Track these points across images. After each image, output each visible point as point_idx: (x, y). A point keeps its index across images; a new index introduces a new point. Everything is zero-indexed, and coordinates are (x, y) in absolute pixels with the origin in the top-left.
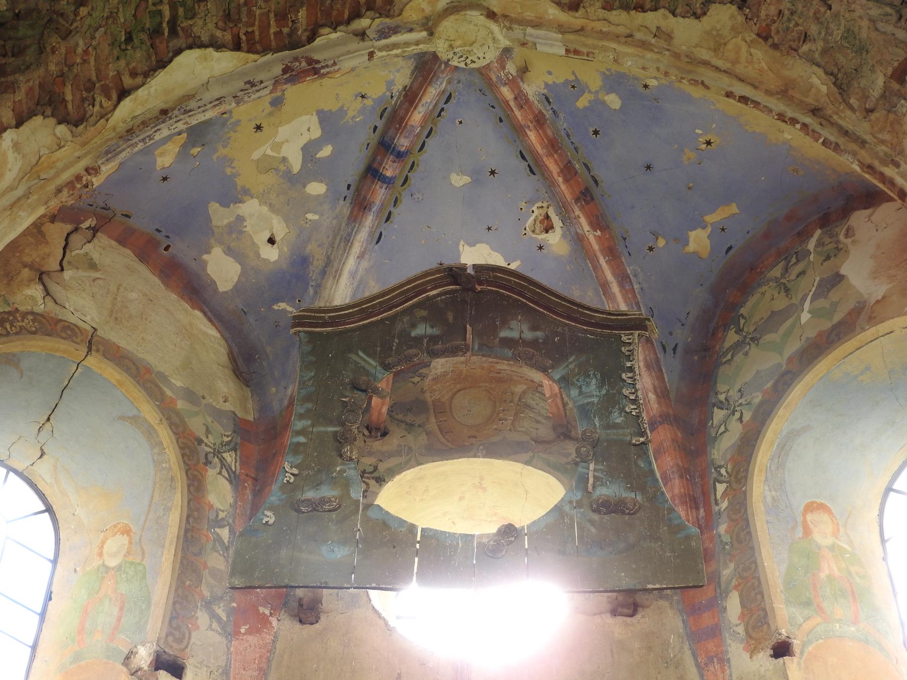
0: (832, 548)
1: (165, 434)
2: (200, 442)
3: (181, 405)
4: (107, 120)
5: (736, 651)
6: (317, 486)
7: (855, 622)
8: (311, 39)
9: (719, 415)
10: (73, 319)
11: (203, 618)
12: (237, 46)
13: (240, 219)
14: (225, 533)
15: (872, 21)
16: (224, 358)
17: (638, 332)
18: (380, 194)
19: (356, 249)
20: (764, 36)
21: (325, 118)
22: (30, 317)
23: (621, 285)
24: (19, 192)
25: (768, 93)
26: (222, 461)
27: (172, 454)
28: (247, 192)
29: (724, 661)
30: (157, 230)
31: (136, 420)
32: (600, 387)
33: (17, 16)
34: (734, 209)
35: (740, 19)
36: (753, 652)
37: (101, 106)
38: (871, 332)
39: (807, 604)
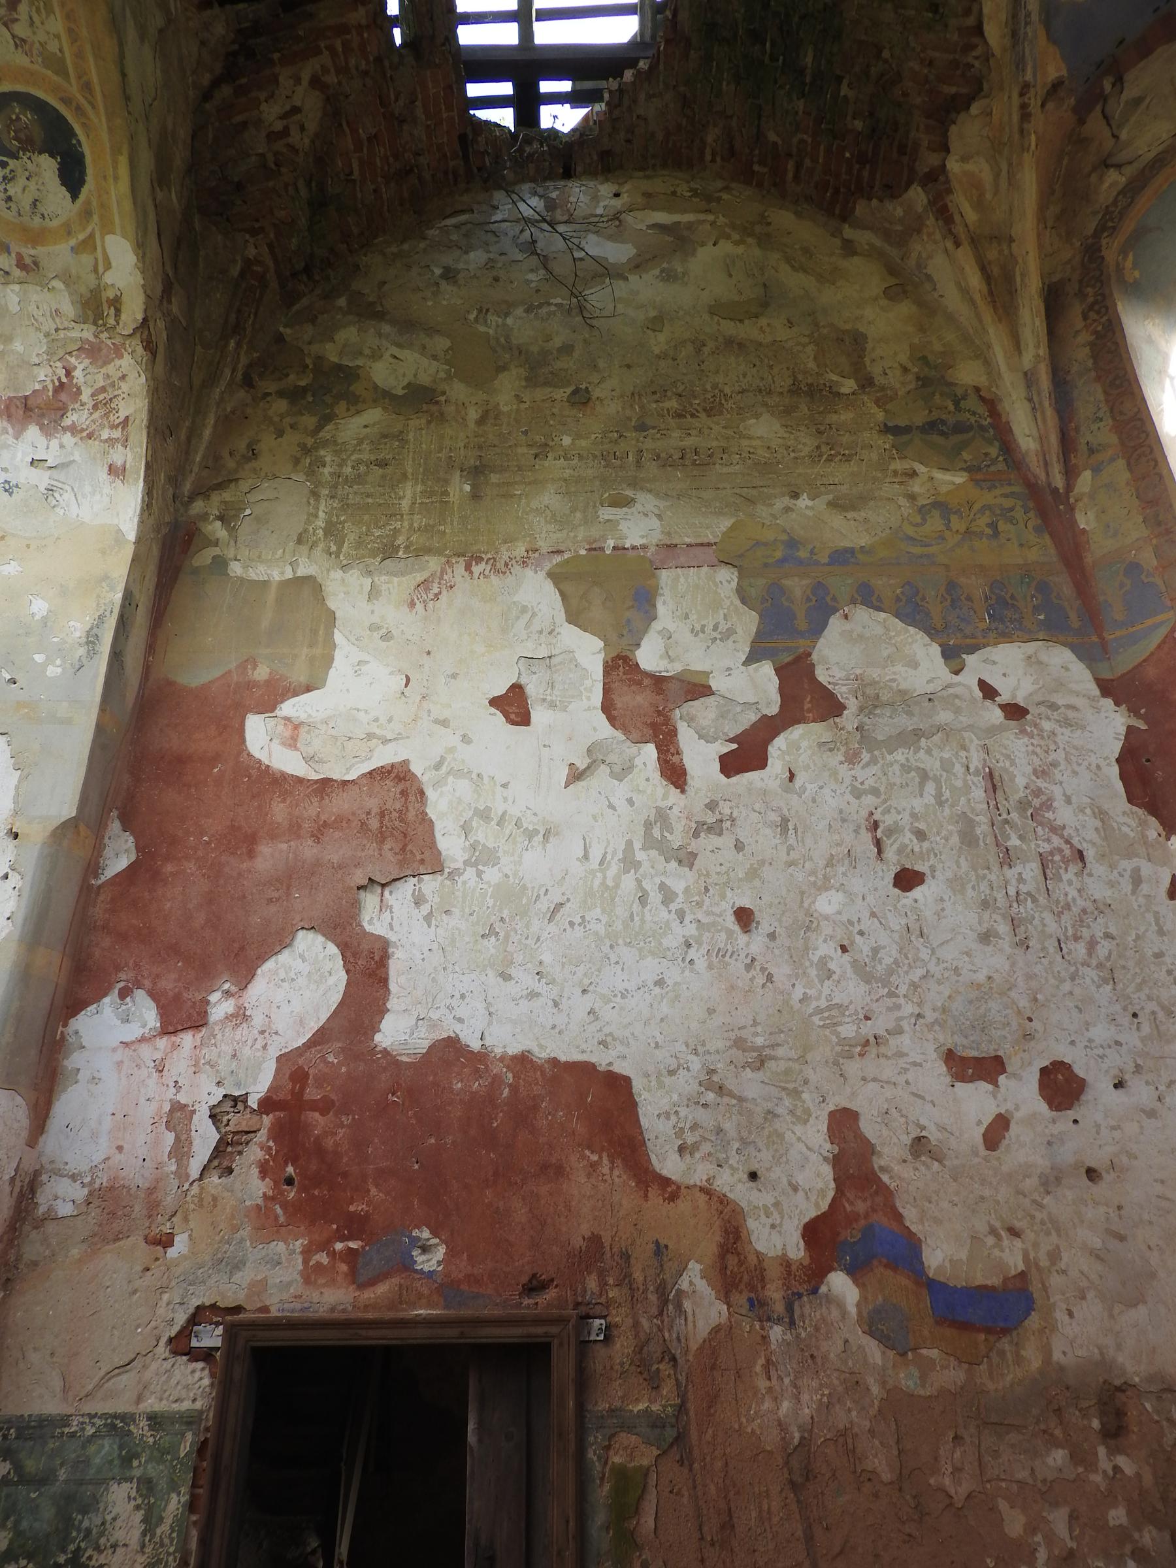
4: (993, 55)
17: (810, 140)
22: (1120, 197)
24: (1004, 166)
30: (1155, 11)
37: (976, 58)
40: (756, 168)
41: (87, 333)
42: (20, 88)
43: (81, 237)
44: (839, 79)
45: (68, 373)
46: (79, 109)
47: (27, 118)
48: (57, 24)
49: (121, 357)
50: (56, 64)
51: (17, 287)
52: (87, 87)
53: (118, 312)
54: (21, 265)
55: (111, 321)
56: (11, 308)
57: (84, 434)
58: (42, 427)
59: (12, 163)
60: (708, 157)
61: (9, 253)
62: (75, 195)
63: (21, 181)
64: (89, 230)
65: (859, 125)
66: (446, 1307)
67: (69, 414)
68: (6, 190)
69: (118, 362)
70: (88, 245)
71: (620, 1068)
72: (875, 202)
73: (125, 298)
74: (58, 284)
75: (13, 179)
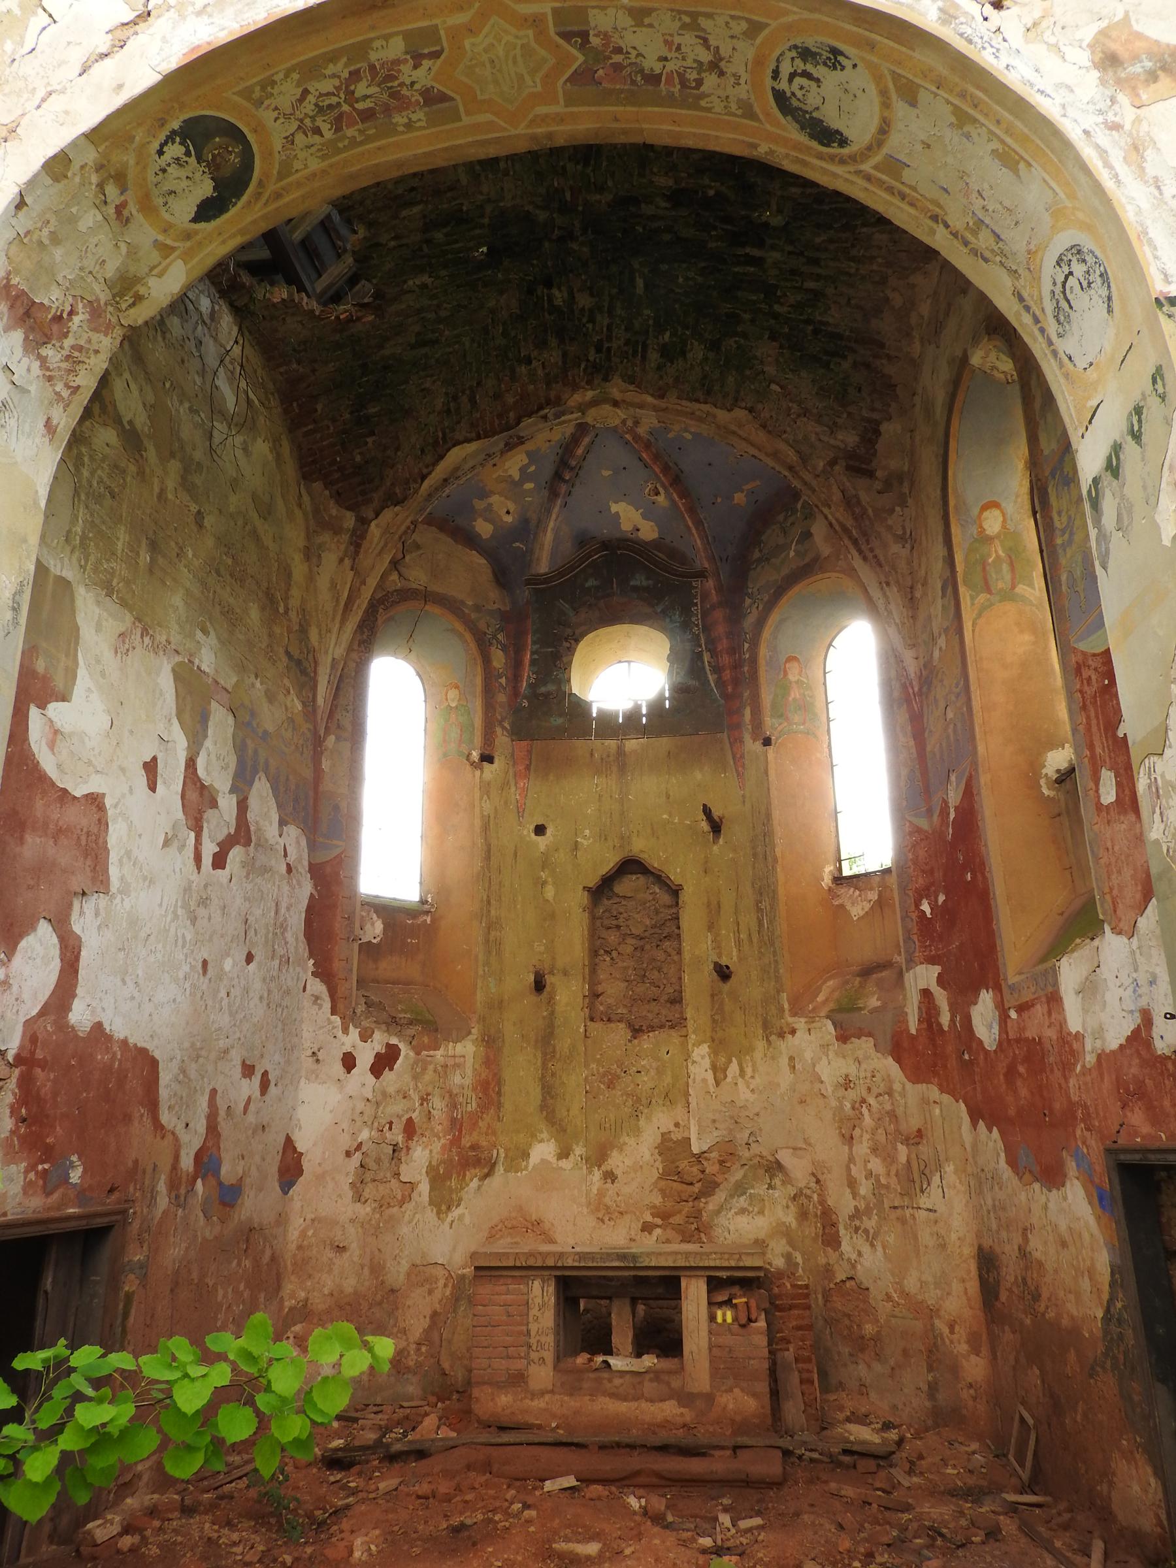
0: (797, 682)
1: (468, 636)
2: (485, 633)
3: (473, 616)
5: (747, 737)
6: (545, 684)
7: (804, 724)
8: (518, 423)
9: (748, 601)
10: (414, 586)
11: (499, 730)
12: (479, 438)
13: (490, 505)
14: (503, 681)
15: (817, 434)
16: (491, 576)
18: (563, 488)
19: (554, 516)
20: (764, 426)
21: (529, 454)
23: (697, 529)
25: (767, 454)
26: (497, 639)
27: (473, 645)
28: (492, 493)
29: (742, 742)
31: (453, 631)
32: (680, 616)
33: (367, 462)
34: (758, 483)
35: (750, 417)
36: (754, 740)
38: (820, 576)
39: (781, 716)
40: (295, 404)
41: (104, 296)
42: (255, 148)
43: (169, 242)
44: (372, 433)
45: (71, 313)
46: (258, 195)
47: (234, 159)
48: (315, 165)
49: (106, 335)
50: (285, 170)
51: (99, 217)
52: (278, 196)
53: (134, 304)
54: (119, 209)
55: (124, 306)
56: (80, 224)
57: (48, 373)
58: (26, 339)
59: (193, 160)
60: (282, 370)
61: (122, 193)
62: (195, 220)
63: (183, 173)
64: (176, 244)
65: (358, 458)
66: (79, 1207)
67: (49, 346)
68: (169, 165)
69: (102, 337)
70: (165, 250)
71: (157, 1054)
72: (327, 493)
73: (145, 303)
74: (124, 248)
75: (181, 165)
